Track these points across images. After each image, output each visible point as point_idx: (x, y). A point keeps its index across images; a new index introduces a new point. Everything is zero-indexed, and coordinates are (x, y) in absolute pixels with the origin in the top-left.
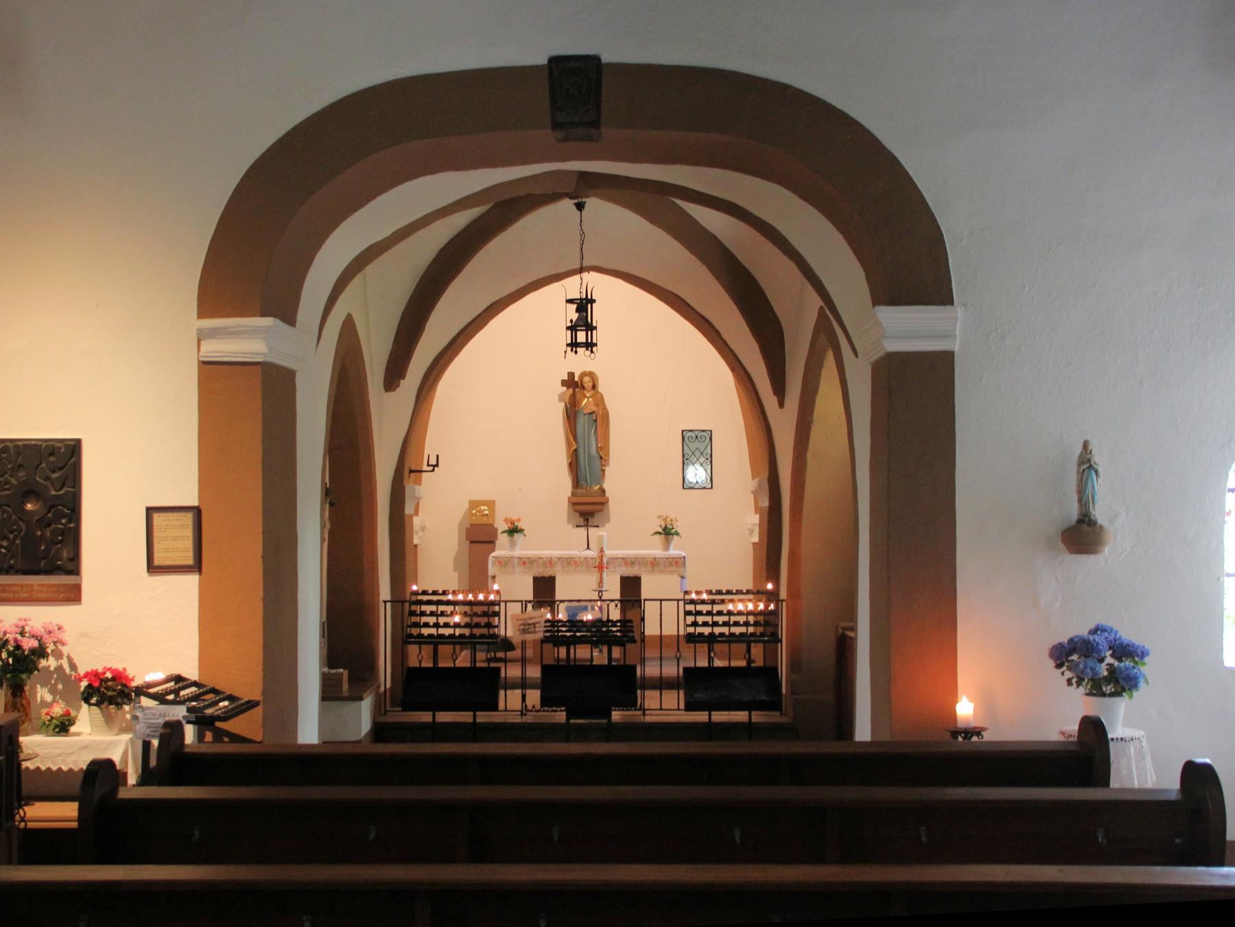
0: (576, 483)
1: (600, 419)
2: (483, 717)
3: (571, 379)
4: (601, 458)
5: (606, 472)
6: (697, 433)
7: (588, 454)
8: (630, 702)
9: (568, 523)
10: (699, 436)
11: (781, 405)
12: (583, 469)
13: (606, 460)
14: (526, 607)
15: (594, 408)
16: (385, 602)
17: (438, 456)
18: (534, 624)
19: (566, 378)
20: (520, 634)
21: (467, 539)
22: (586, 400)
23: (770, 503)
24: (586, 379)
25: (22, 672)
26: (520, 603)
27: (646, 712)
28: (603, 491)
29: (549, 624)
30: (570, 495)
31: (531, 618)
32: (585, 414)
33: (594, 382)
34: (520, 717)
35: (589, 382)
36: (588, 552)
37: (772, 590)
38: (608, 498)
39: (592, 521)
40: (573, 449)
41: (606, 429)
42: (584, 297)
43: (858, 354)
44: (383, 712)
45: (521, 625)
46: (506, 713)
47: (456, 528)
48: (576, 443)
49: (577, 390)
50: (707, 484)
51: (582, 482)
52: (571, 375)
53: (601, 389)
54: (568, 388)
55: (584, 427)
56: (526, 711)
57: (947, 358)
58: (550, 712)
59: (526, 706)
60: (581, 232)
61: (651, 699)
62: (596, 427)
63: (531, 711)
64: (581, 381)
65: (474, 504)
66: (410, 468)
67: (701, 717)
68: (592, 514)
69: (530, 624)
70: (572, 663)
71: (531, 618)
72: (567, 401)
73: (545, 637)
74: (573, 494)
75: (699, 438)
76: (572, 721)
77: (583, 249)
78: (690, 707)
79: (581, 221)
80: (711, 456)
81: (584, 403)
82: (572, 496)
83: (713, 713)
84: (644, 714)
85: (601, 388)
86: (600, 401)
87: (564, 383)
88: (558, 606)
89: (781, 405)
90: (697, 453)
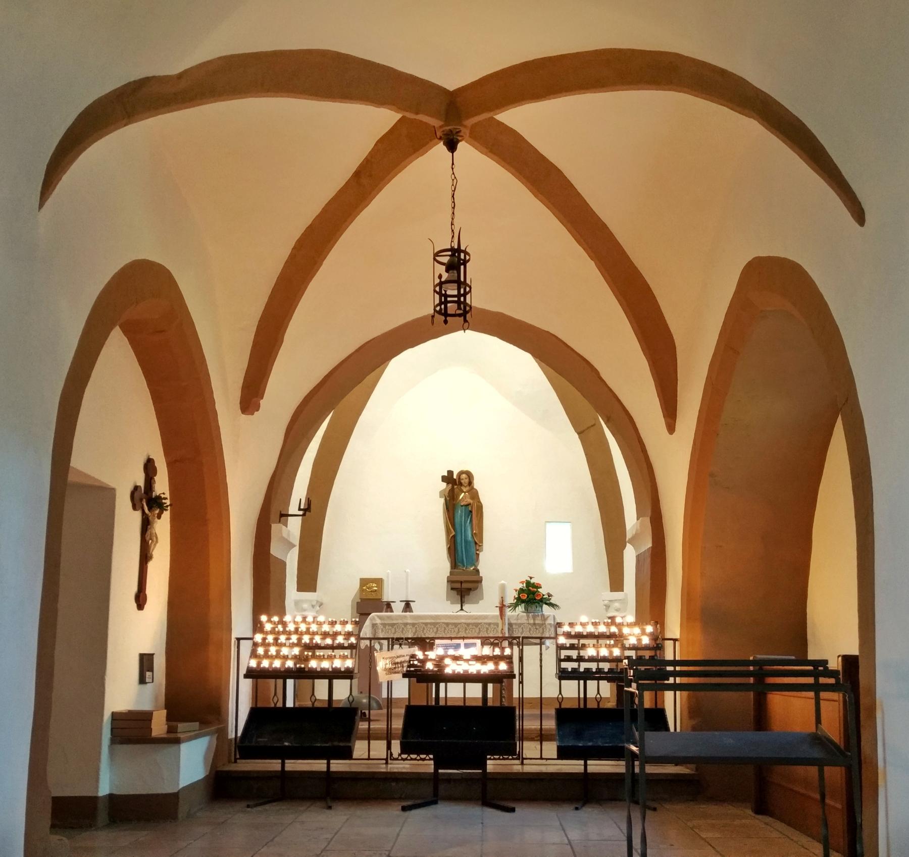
1: (474, 511)
2: (338, 765)
4: (476, 543)
8: (509, 750)
9: (447, 600)
11: (671, 428)
12: (459, 548)
13: (480, 546)
15: (469, 501)
16: (239, 639)
17: (401, 601)
18: (401, 663)
19: (446, 475)
20: (386, 674)
21: (357, 612)
22: (463, 494)
23: (653, 542)
27: (525, 761)
28: (478, 571)
31: (398, 657)
32: (462, 506)
33: (469, 479)
34: (384, 766)
35: (466, 478)
40: (451, 536)
41: (480, 518)
42: (456, 247)
43: (868, 217)
44: (233, 760)
46: (370, 761)
47: (350, 603)
48: (454, 530)
49: (455, 487)
51: (459, 564)
52: (450, 473)
54: (448, 484)
55: (461, 517)
56: (391, 759)
58: (418, 760)
59: (391, 755)
60: (453, 178)
61: (530, 749)
63: (397, 759)
64: (459, 478)
65: (364, 582)
66: (281, 512)
67: (574, 766)
68: (469, 590)
69: (398, 663)
70: (442, 703)
71: (398, 657)
72: (447, 495)
73: (407, 671)
76: (440, 771)
77: (455, 196)
78: (564, 753)
79: (453, 164)
81: (461, 497)
82: (450, 575)
83: (589, 762)
84: (522, 764)
85: (477, 484)
86: (475, 495)
87: (444, 479)
89: (671, 428)
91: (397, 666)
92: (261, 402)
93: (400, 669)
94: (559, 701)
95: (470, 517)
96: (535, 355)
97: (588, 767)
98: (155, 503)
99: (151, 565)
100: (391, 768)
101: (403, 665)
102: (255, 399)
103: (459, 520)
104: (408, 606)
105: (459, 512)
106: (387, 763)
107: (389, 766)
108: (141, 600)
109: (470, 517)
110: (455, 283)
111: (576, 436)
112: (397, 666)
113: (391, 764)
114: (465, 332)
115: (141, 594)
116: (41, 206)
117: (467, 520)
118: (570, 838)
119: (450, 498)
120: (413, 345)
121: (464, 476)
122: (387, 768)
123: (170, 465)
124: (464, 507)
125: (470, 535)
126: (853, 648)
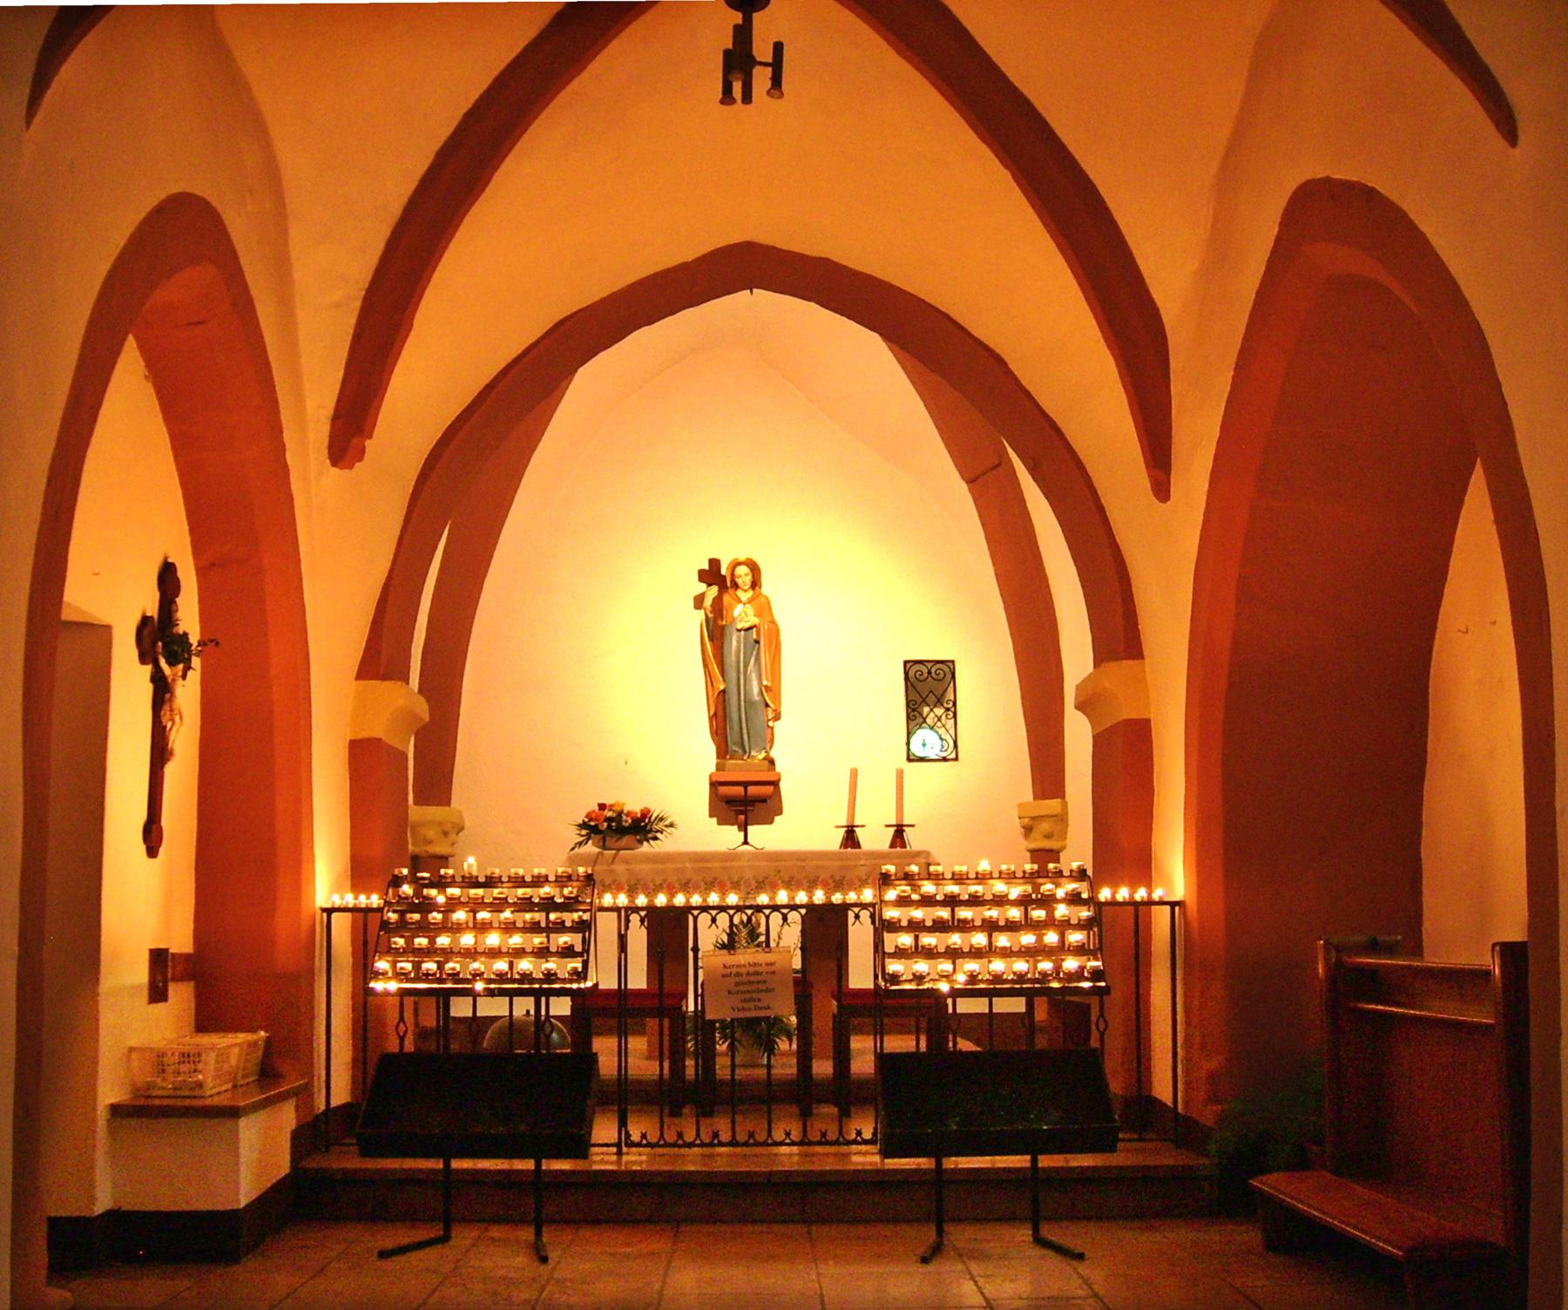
0: (723, 752)
1: (765, 639)
3: (714, 569)
5: (776, 731)
6: (929, 665)
9: (711, 816)
10: (933, 670)
11: (1162, 491)
12: (735, 716)
14: (628, 921)
15: (754, 620)
19: (706, 567)
24: (742, 571)
26: (615, 915)
28: (772, 762)
29: (737, 88)
30: (713, 769)
32: (739, 631)
33: (753, 576)
35: (747, 575)
36: (746, 847)
37: (1144, 886)
38: (779, 774)
43: (1522, 125)
48: (723, 676)
50: (949, 751)
52: (714, 563)
53: (767, 587)
57: (1148, 721)
58: (680, 1146)
59: (628, 1135)
63: (639, 1145)
64: (733, 575)
74: (719, 767)
75: (933, 674)
80: (955, 704)
87: (703, 576)
88: (695, 919)
89: (1162, 491)
90: (932, 699)
92: (366, 444)
96: (886, 337)
98: (178, 650)
99: (170, 771)
100: (626, 1163)
102: (354, 441)
106: (619, 1153)
107: (625, 1158)
108: (152, 836)
109: (755, 653)
111: (964, 487)
113: (627, 1154)
114: (752, 292)
115: (154, 826)
116: (28, 123)
117: (750, 659)
118: (987, 1295)
119: (714, 614)
120: (650, 321)
121: (742, 571)
122: (619, 1162)
123: (201, 572)
124: (743, 632)
125: (756, 690)
126: (1514, 930)
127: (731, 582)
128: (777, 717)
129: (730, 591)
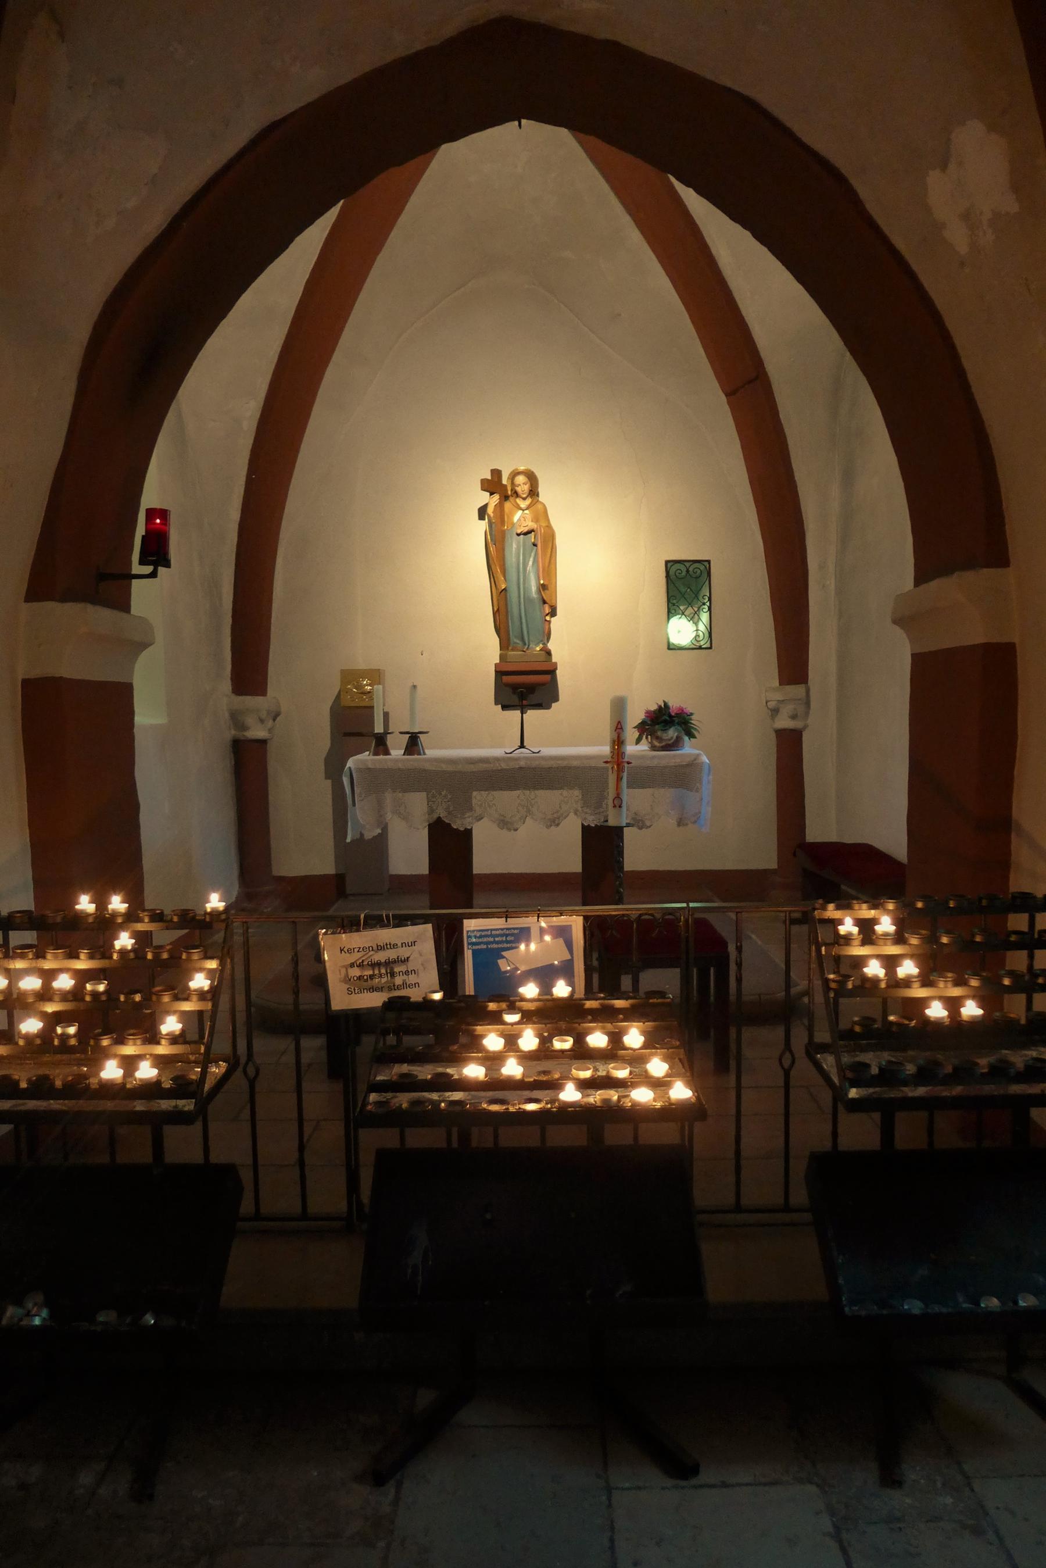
0: (505, 644)
7: (524, 588)
10: (691, 569)
17: (401, 733)
18: (388, 963)
25: (104, 911)
28: (549, 653)
32: (518, 535)
33: (531, 485)
38: (556, 664)
39: (534, 698)
45: (352, 965)
52: (496, 473)
62: (536, 554)
64: (513, 483)
69: (378, 964)
80: (710, 599)
91: (377, 972)
93: (384, 980)
94: (783, 1067)
95: (358, 1110)
97: (782, 1084)
101: (392, 969)
103: (514, 560)
104: (413, 743)
105: (514, 546)
110: (8, 935)
112: (377, 972)
121: (521, 479)
127: (512, 490)
128: (553, 613)
129: (511, 499)
